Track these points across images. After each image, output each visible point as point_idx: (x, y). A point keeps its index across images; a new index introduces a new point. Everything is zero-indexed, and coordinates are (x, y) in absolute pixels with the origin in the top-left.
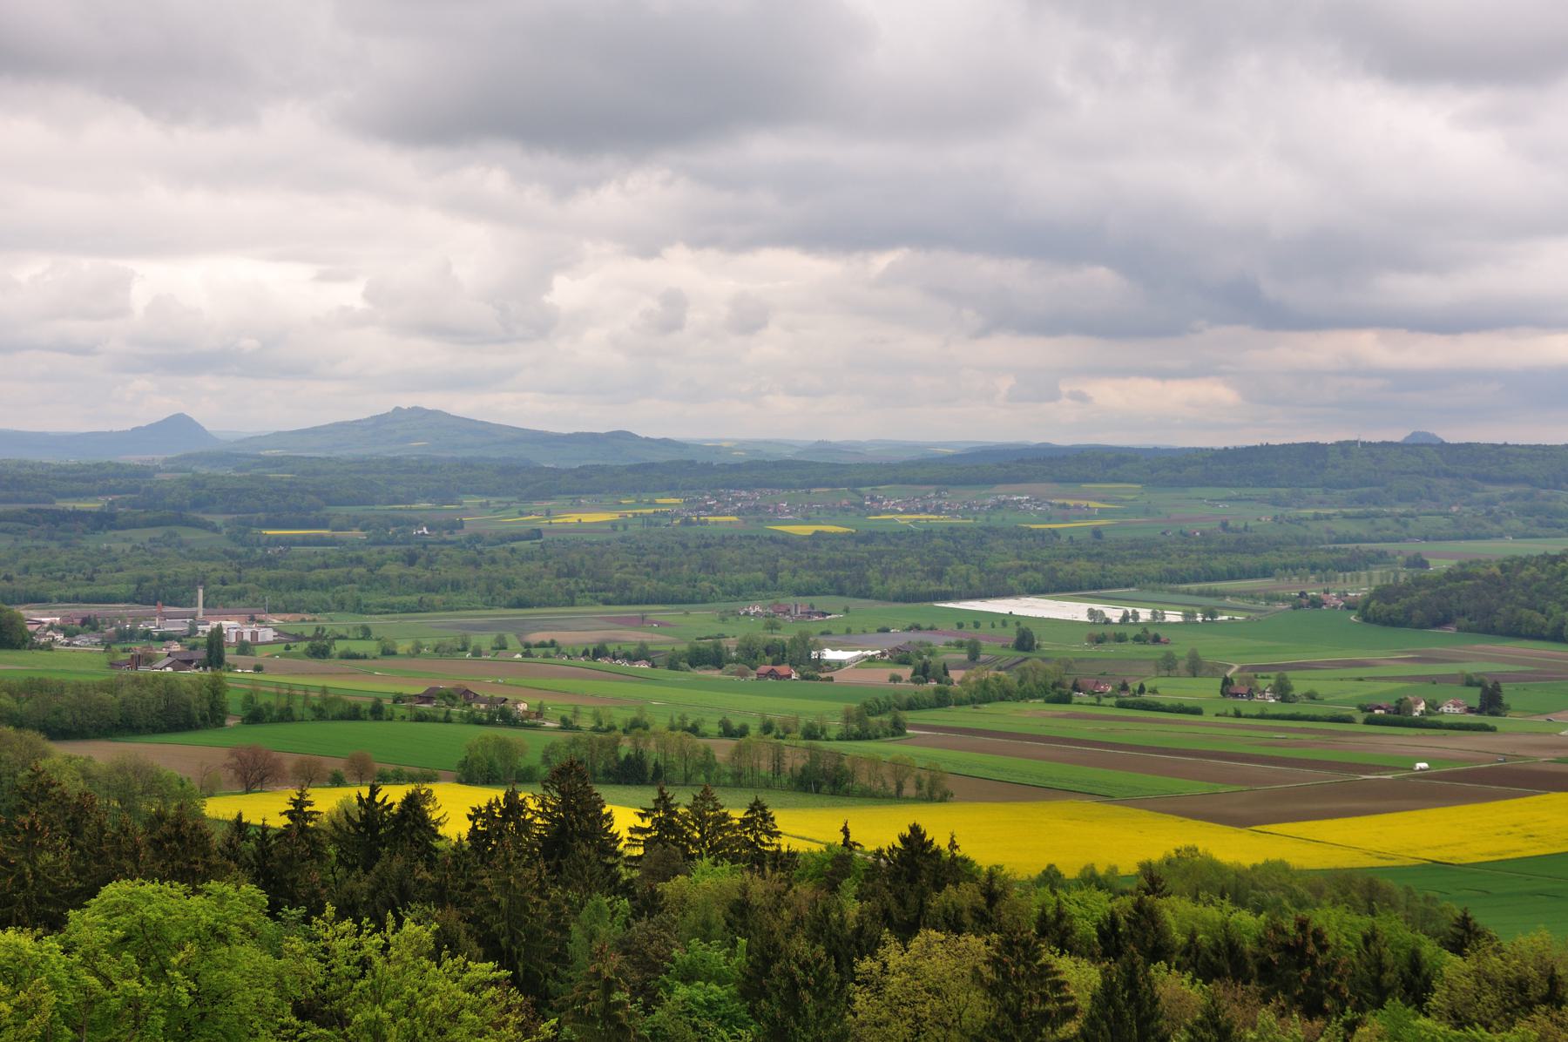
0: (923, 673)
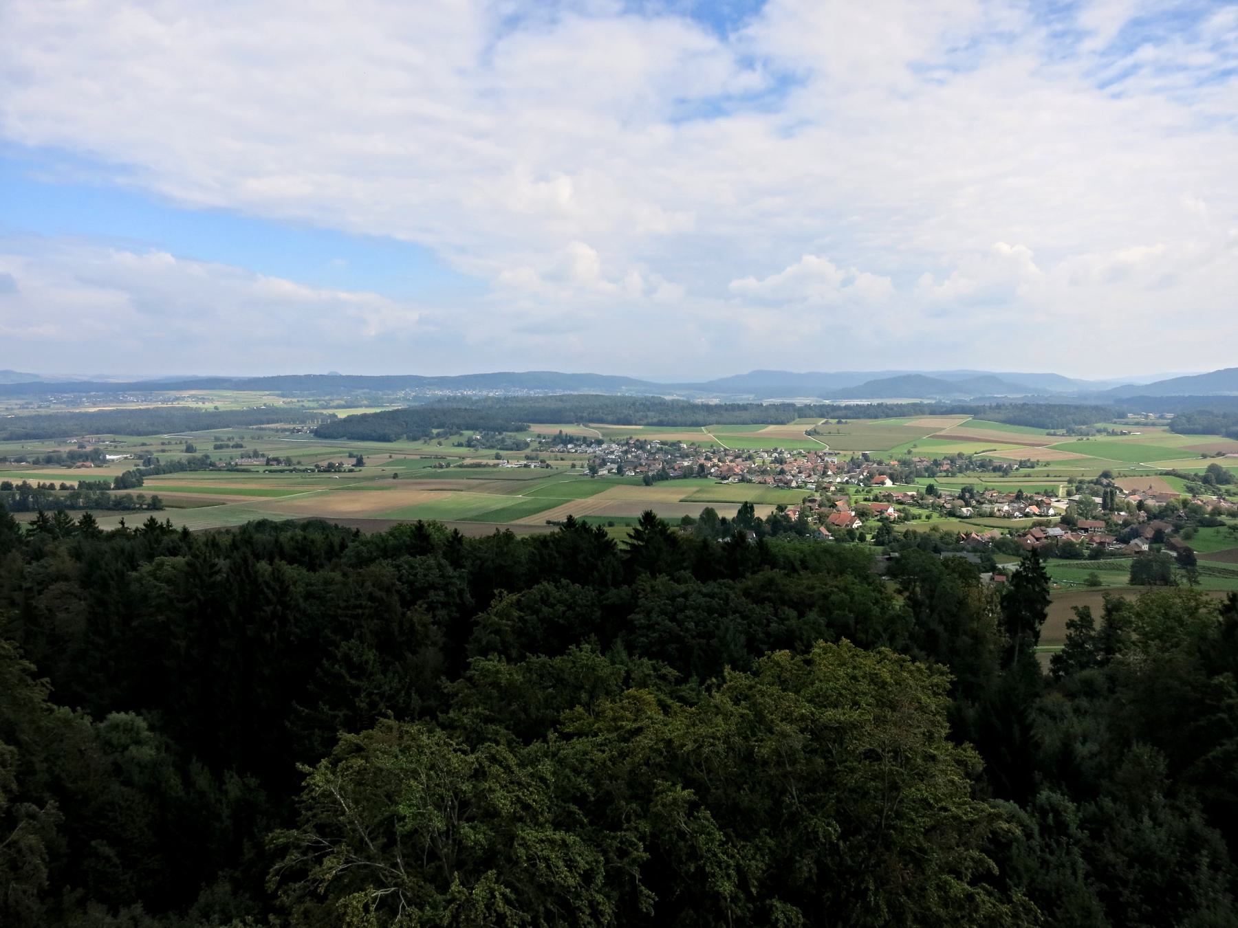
0: (148, 462)
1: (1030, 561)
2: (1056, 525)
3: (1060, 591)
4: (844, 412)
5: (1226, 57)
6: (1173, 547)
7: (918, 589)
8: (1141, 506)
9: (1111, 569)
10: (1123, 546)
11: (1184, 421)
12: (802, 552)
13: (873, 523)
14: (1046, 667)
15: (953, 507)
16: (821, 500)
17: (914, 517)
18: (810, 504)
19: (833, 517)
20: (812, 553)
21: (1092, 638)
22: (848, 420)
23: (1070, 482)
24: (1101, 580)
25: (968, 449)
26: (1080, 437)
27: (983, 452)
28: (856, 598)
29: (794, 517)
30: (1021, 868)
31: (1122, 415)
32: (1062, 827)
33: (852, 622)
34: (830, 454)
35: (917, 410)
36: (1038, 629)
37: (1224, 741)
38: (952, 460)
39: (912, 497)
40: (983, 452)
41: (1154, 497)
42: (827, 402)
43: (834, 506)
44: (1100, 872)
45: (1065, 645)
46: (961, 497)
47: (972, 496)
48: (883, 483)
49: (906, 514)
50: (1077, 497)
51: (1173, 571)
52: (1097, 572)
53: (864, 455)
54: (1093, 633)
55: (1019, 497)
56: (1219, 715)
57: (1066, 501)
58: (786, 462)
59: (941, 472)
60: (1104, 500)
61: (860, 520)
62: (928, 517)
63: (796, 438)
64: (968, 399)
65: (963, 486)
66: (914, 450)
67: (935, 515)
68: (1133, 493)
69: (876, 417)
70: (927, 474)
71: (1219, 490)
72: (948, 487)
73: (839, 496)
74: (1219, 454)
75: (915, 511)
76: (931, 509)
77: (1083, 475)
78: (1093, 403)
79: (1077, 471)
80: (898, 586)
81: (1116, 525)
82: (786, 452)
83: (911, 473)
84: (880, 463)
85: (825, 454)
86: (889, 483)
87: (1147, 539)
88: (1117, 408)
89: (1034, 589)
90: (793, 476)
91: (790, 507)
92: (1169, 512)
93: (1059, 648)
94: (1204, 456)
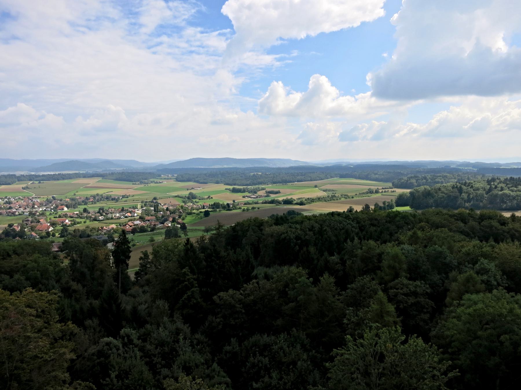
1: (122, 236)
2: (137, 220)
3: (140, 246)
4: (42, 178)
5: (191, 46)
6: (178, 223)
7: (74, 255)
8: (167, 209)
9: (158, 234)
10: (162, 225)
11: (181, 177)
12: (13, 246)
13: (59, 228)
14: (132, 277)
15: (95, 217)
16: (32, 220)
17: (78, 223)
18: (26, 222)
19: (39, 226)
20: (19, 246)
21: (149, 262)
22: (44, 182)
23: (142, 202)
24: (155, 239)
25: (100, 192)
26: (145, 185)
27: (108, 192)
28: (40, 264)
29: (18, 229)
30: (115, 364)
31: (160, 176)
32: (131, 341)
33: (39, 276)
34: (35, 198)
35: (77, 176)
36: (128, 263)
37: (187, 292)
38: (94, 197)
39: (77, 214)
40: (108, 192)
41: (172, 206)
42: (33, 173)
43: (39, 222)
44: (146, 354)
45: (139, 267)
46: (99, 212)
47: (103, 212)
48: (63, 209)
49: (75, 222)
50: (144, 208)
51: (179, 232)
52: (153, 236)
53: (53, 197)
54: (149, 260)
55: (123, 210)
56: (185, 283)
57: (141, 210)
58: (12, 203)
59: (89, 202)
60: (155, 208)
61: (52, 227)
62: (85, 222)
63: (17, 191)
64: (100, 171)
65: (99, 208)
66: (77, 194)
67: (88, 221)
68: (165, 205)
69: (58, 180)
70: (83, 204)
71: (193, 201)
72: (93, 208)
73: (41, 217)
74: (192, 188)
75: (78, 220)
76: (86, 219)
77: (147, 199)
78: (149, 171)
79: (144, 198)
80: (65, 255)
81: (159, 217)
82: (12, 198)
83: (76, 204)
84: (61, 200)
85: (33, 198)
86: (66, 209)
87: (170, 221)
88: (158, 173)
89: (125, 247)
90: (16, 210)
91: (15, 225)
92: (177, 211)
93: (137, 269)
94: (188, 190)
